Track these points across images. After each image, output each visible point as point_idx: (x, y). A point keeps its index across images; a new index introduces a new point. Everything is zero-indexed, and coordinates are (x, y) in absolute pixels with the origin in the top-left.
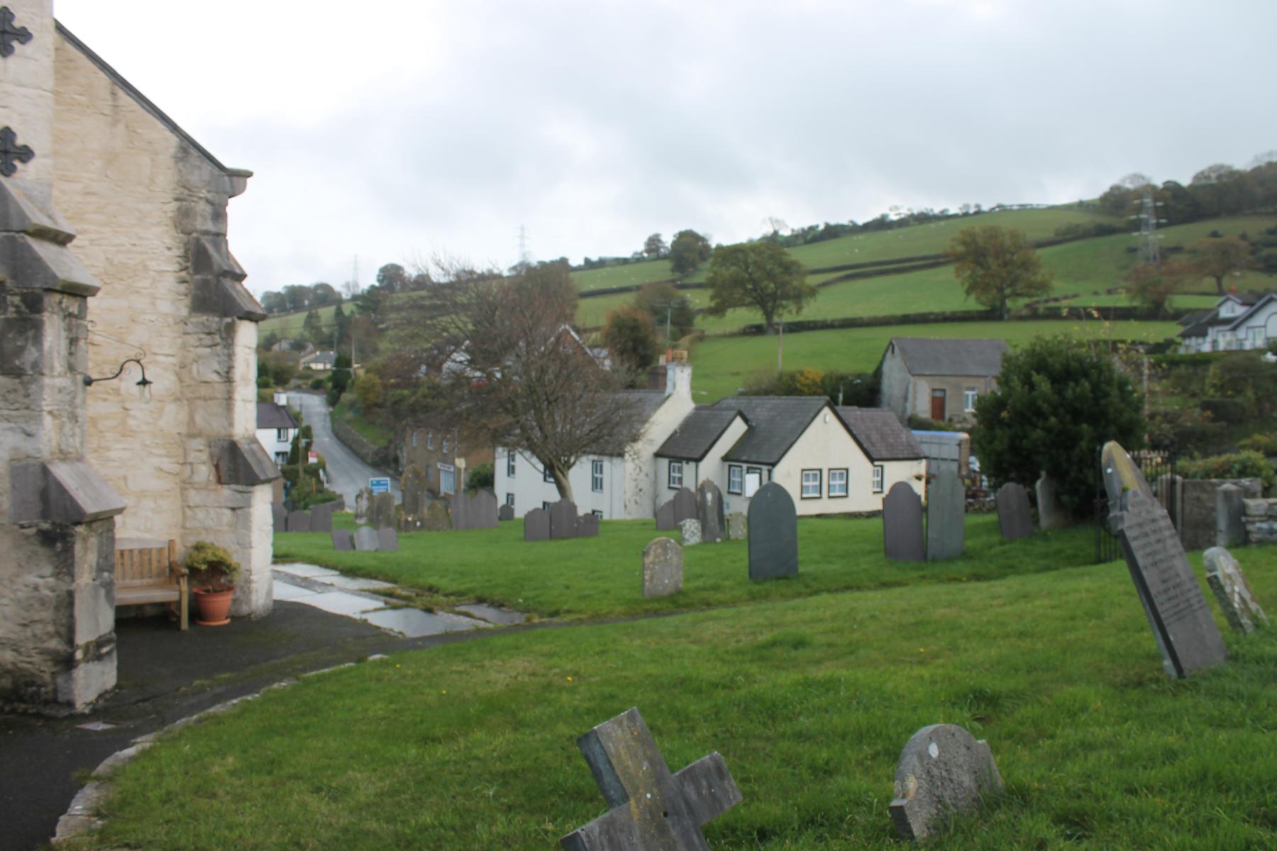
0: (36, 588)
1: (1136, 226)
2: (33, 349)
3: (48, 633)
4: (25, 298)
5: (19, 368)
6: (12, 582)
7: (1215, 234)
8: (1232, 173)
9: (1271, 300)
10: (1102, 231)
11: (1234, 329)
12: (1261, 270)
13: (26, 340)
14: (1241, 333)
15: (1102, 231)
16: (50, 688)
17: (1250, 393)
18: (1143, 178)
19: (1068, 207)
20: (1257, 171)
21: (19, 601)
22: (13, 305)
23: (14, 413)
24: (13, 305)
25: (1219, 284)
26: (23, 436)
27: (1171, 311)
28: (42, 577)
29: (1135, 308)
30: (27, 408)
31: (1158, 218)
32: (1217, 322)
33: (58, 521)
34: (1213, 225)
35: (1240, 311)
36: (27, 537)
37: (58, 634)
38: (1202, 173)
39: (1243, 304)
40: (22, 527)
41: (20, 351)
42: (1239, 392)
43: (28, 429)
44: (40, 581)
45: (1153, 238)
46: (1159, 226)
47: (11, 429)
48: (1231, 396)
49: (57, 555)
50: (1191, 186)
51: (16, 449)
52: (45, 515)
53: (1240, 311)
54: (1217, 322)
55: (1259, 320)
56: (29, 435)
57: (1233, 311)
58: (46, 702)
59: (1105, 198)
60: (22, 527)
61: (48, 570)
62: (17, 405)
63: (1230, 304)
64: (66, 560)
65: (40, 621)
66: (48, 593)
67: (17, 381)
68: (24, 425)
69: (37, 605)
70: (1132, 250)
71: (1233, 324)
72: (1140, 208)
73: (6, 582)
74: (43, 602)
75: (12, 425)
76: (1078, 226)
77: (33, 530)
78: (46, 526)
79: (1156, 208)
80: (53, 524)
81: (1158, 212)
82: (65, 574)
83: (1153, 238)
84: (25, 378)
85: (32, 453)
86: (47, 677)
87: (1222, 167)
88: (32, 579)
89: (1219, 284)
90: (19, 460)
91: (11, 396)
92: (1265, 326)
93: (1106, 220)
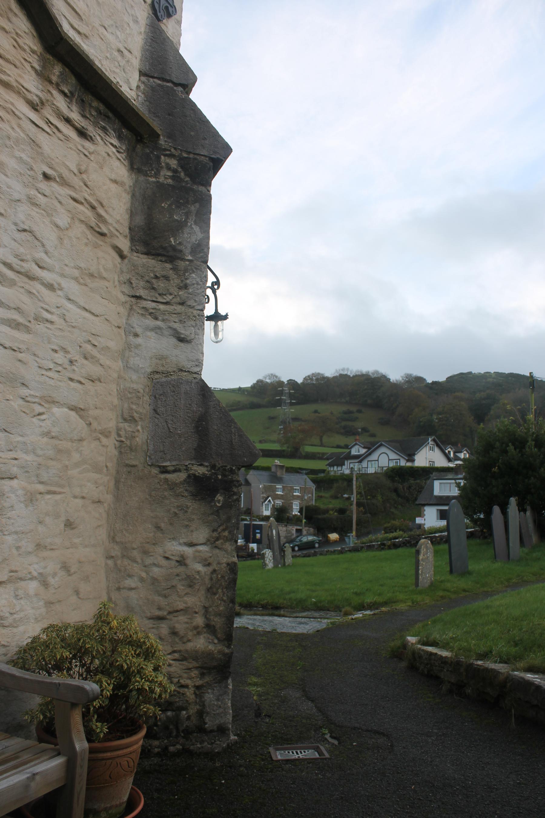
0: (182, 561)
1: (279, 403)
2: (196, 229)
3: (196, 628)
4: (184, 163)
5: (174, 249)
6: (146, 553)
7: (316, 412)
8: (324, 378)
9: (381, 445)
10: (254, 406)
11: (360, 462)
12: (342, 434)
13: (187, 214)
14: (364, 464)
15: (254, 406)
16: (193, 710)
17: (379, 498)
18: (276, 377)
19: (233, 391)
20: (335, 378)
21: (155, 581)
22: (169, 168)
23: (162, 307)
24: (169, 168)
25: (321, 440)
26: (174, 341)
27: (304, 454)
28: (191, 545)
29: (284, 451)
30: (182, 304)
31: (291, 400)
32: (349, 457)
33: (219, 463)
34: (313, 407)
35: (363, 451)
36: (172, 486)
37: (210, 628)
38: (309, 376)
39: (364, 448)
40: (164, 470)
41: (180, 226)
42: (374, 497)
43: (184, 332)
44: (188, 551)
45: (287, 411)
46: (291, 404)
47: (156, 329)
48: (370, 499)
49: (217, 512)
50: (302, 383)
51: (162, 358)
52: (200, 454)
53: (363, 451)
54: (349, 457)
55: (374, 456)
56: (182, 340)
57: (359, 452)
58: (188, 733)
59: (254, 387)
60: (164, 470)
61: (202, 534)
62: (169, 298)
63: (357, 447)
64: (229, 519)
65: (185, 611)
66: (199, 567)
67: (168, 266)
68: (176, 326)
69: (180, 587)
70: (271, 418)
71: (360, 458)
72: (281, 393)
73: (135, 554)
74: (190, 582)
75: (159, 323)
76: (239, 402)
77: (183, 476)
78: (201, 470)
79: (290, 393)
80: (213, 467)
81: (291, 396)
82: (227, 539)
83: (287, 411)
84: (182, 264)
85: (187, 365)
86: (190, 693)
87: (319, 374)
88: (175, 548)
89: (321, 440)
90: (167, 374)
91: (161, 285)
92: (378, 460)
93: (255, 400)
